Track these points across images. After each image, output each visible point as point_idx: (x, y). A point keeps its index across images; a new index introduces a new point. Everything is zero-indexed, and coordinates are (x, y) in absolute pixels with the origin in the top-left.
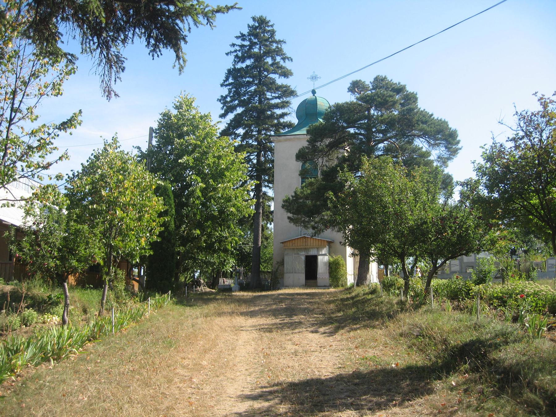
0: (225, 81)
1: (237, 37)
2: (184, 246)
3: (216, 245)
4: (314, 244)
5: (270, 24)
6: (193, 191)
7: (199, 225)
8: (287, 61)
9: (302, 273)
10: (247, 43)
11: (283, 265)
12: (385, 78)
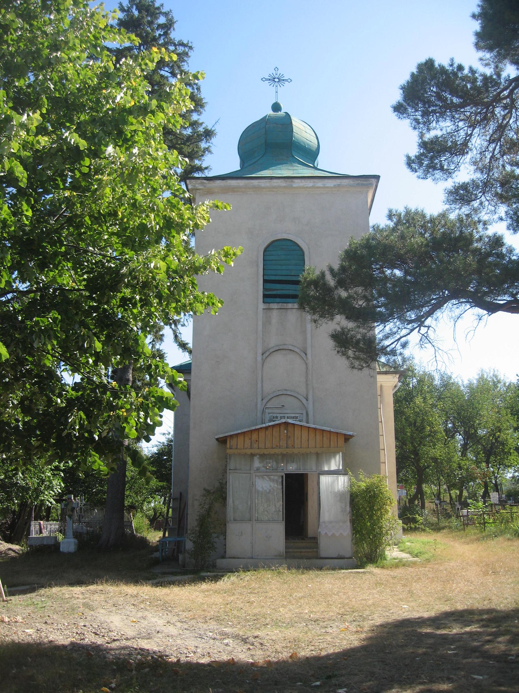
3: (76, 418)
9: (274, 521)
11: (225, 499)
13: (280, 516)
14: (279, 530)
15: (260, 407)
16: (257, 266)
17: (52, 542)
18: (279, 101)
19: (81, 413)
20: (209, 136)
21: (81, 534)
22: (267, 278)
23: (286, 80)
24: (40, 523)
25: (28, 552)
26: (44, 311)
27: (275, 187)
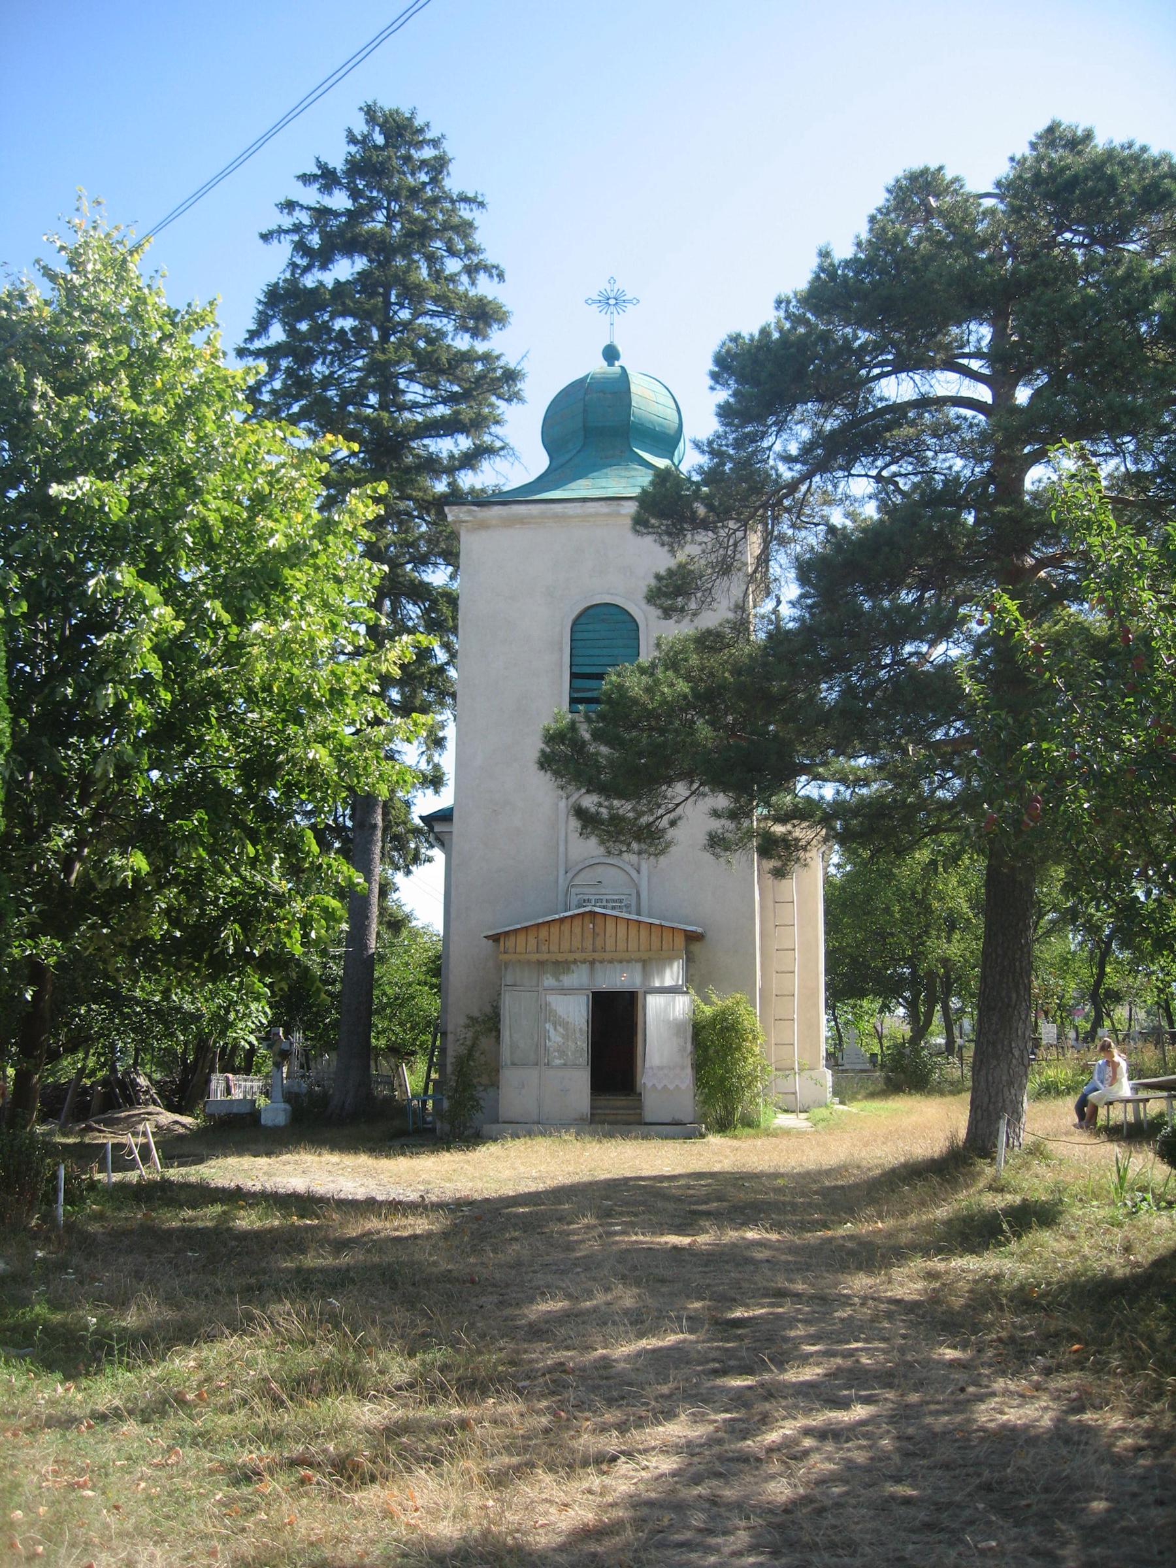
0: (253, 335)
1: (306, 179)
2: (63, 934)
3: (230, 933)
4: (633, 945)
5: (429, 135)
6: (121, 649)
7: (147, 834)
8: (482, 277)
9: (575, 1066)
10: (340, 201)
12: (1088, 136)
13: (584, 1058)
14: (580, 1080)
15: (562, 883)
16: (561, 650)
17: (245, 1109)
18: (616, 343)
19: (237, 926)
20: (514, 380)
21: (298, 1095)
22: (576, 670)
23: (630, 301)
24: (227, 1080)
25: (206, 1128)
26: (186, 814)
27: (590, 515)
